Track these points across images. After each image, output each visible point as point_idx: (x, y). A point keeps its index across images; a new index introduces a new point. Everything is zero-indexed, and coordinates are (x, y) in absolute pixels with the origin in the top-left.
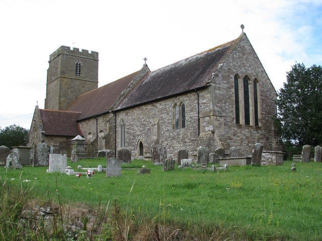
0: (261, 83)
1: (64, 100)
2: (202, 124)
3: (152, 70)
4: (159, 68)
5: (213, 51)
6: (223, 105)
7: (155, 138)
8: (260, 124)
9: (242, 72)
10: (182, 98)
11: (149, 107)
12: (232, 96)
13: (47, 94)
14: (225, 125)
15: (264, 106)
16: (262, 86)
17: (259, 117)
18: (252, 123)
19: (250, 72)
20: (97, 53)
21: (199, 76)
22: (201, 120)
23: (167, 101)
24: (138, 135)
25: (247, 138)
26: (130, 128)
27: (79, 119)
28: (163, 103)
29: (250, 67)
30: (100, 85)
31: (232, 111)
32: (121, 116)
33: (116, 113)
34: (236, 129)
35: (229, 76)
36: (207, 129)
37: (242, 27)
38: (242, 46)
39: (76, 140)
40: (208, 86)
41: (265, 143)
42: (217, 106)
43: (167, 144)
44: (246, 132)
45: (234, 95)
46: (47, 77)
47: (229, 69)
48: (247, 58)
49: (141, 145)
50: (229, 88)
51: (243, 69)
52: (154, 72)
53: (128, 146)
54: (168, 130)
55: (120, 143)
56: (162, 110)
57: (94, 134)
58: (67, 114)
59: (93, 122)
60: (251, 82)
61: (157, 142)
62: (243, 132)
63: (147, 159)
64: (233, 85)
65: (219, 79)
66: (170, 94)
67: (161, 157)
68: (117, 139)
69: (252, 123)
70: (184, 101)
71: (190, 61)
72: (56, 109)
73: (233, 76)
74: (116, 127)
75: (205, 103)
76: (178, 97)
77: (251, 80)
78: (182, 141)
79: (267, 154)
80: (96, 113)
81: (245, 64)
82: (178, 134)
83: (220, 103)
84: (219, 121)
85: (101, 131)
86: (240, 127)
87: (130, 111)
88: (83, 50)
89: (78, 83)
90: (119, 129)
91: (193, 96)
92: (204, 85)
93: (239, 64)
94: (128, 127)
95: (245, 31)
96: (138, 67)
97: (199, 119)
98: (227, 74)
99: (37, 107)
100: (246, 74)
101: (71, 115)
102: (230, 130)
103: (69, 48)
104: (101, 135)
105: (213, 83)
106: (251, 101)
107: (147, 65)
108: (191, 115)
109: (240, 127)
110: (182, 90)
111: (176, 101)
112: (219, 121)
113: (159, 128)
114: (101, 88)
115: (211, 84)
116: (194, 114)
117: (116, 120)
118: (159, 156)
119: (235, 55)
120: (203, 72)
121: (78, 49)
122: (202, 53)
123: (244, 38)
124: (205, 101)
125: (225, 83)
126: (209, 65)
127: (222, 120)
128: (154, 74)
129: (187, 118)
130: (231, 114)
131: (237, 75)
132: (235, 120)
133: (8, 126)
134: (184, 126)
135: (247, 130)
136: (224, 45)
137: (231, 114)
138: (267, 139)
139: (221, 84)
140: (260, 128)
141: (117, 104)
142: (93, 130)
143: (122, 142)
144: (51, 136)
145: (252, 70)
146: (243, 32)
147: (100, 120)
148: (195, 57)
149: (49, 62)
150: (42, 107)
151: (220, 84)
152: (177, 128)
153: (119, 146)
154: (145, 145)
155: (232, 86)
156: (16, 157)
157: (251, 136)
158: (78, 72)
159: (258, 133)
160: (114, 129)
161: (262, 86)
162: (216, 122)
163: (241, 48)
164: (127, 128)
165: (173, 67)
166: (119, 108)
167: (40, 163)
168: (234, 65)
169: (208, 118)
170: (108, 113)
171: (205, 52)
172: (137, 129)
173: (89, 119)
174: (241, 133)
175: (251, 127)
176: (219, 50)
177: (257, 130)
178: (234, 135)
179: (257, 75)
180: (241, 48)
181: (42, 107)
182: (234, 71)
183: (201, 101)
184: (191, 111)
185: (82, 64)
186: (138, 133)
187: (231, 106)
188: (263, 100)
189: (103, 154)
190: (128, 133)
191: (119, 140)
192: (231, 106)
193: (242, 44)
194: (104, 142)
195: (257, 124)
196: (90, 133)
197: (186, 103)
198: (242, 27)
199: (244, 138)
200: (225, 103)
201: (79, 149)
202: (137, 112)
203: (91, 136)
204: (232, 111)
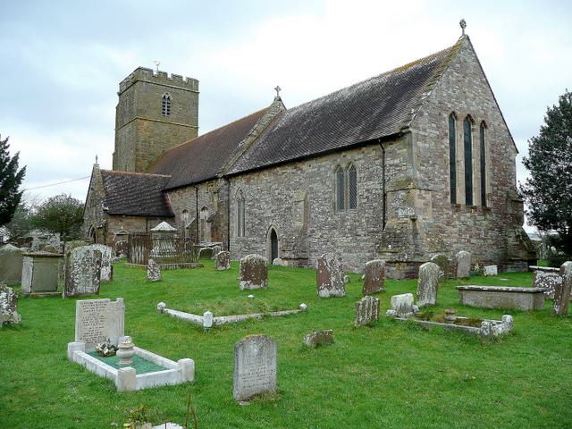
0: (491, 129)
2: (391, 204)
3: (288, 107)
7: (299, 224)
8: (489, 205)
9: (462, 108)
10: (349, 156)
11: (289, 170)
13: (116, 146)
14: (434, 205)
16: (494, 134)
17: (488, 190)
18: (476, 201)
19: (475, 109)
20: (197, 82)
21: (381, 116)
22: (389, 196)
23: (323, 159)
25: (468, 229)
27: (167, 187)
28: (314, 163)
30: (201, 133)
31: (444, 180)
32: (239, 184)
33: (228, 178)
36: (400, 213)
37: (463, 24)
39: (159, 231)
40: (404, 134)
41: (497, 237)
42: (421, 171)
44: (466, 217)
45: (448, 151)
46: (117, 118)
48: (470, 82)
49: (274, 235)
50: (440, 138)
51: (463, 102)
52: (293, 110)
53: (251, 235)
54: (323, 212)
55: (236, 229)
56: (311, 176)
57: (192, 213)
58: (148, 179)
59: (190, 192)
60: (476, 127)
61: (303, 232)
62: (462, 218)
63: (286, 263)
64: (448, 131)
65: (424, 121)
66: (329, 147)
67: (333, 279)
68: (231, 222)
69: (476, 201)
72: (130, 171)
73: (446, 116)
74: (228, 202)
75: (397, 166)
76: (343, 154)
77: (477, 126)
78: (350, 233)
79: (554, 274)
80: (196, 177)
82: (344, 221)
85: (203, 209)
86: (457, 208)
87: (255, 177)
88: (174, 76)
89: (166, 128)
90: (234, 206)
91: (372, 152)
95: (467, 31)
96: (265, 102)
97: (385, 195)
99: (96, 165)
100: (468, 112)
101: (155, 181)
103: (151, 71)
104: (204, 215)
105: (414, 128)
106: (475, 162)
107: (280, 100)
108: (368, 187)
109: (457, 208)
110: (350, 141)
111: (338, 160)
112: (424, 198)
113: (306, 206)
114: (203, 136)
115: (410, 129)
116: (375, 185)
117: (229, 190)
118: (329, 276)
120: (390, 108)
121: (165, 74)
122: (381, 76)
123: (465, 45)
124: (397, 161)
125: (433, 128)
126: (400, 95)
127: (429, 196)
128: (292, 114)
129: (359, 192)
130: (443, 186)
132: (449, 197)
133: (53, 195)
134: (353, 206)
135: (468, 215)
136: (425, 60)
138: (501, 230)
140: (489, 210)
141: (231, 163)
142: (191, 205)
143: (239, 229)
144: (121, 215)
145: (478, 104)
146: (463, 34)
147: (203, 190)
148: (369, 83)
149: (120, 95)
150: (107, 164)
151: (425, 130)
152: (341, 207)
153: (235, 235)
154: (280, 235)
155: (446, 134)
157: (475, 224)
158: (166, 111)
160: (225, 206)
161: (494, 134)
162: (419, 200)
163: (458, 61)
165: (328, 101)
166: (235, 171)
168: (449, 95)
169: (403, 193)
170: (216, 178)
171: (388, 73)
172: (266, 209)
173: (183, 187)
174: (459, 219)
175: (475, 208)
177: (484, 215)
178: (448, 224)
180: (458, 61)
181: (107, 164)
183: (389, 161)
184: (369, 179)
185: (171, 98)
187: (442, 171)
188: (494, 160)
189: (208, 254)
190: (250, 214)
191: (234, 225)
193: (462, 55)
194: (208, 228)
195: (484, 203)
196: (184, 211)
197: (359, 164)
198: (463, 24)
201: (164, 247)
202: (266, 177)
203: (186, 216)
204: (444, 180)
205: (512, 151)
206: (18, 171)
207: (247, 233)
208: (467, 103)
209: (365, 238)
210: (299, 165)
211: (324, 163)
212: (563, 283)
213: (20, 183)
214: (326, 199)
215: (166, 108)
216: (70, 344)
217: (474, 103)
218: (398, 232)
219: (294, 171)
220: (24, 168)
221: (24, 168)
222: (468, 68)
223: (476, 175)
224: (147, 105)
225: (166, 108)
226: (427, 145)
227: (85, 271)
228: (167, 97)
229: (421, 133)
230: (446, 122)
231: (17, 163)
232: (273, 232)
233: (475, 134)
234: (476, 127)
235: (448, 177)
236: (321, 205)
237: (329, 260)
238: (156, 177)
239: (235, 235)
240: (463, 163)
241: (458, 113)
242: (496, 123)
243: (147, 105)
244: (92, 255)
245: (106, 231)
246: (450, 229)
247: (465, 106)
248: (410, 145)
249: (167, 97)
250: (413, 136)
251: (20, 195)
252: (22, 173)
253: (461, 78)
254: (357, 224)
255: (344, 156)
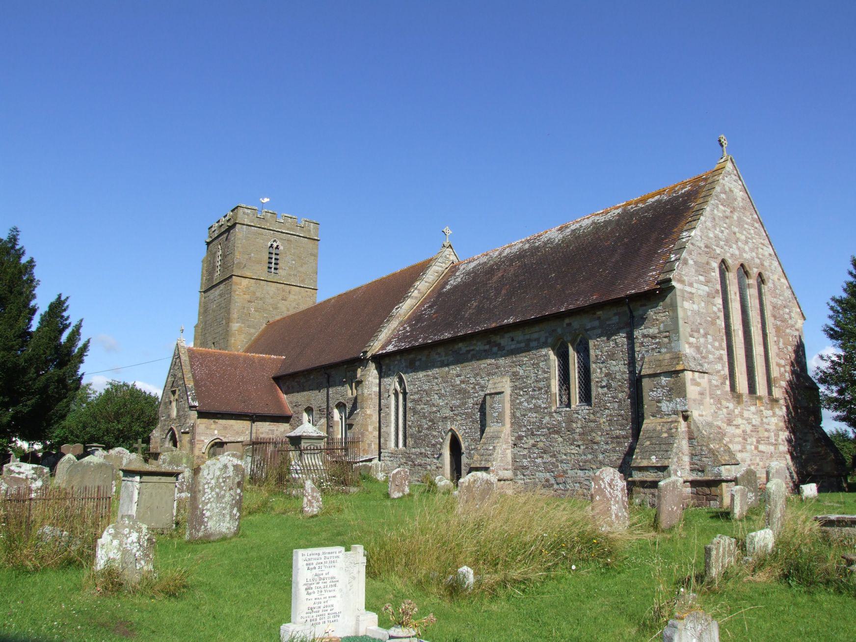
0: (770, 284)
1: (241, 327)
4: (197, 313)
5: (641, 205)
6: (702, 340)
9: (733, 254)
12: (718, 318)
15: (781, 345)
18: (761, 389)
24: (445, 418)
25: (755, 429)
26: (420, 400)
29: (746, 243)
34: (731, 406)
35: (708, 263)
36: (665, 406)
38: (727, 189)
43: (534, 445)
44: (751, 411)
45: (721, 315)
47: (706, 247)
48: (739, 218)
50: (710, 296)
62: (746, 414)
70: (588, 330)
71: (573, 231)
73: (715, 265)
75: (654, 337)
76: (567, 321)
81: (738, 234)
83: (695, 334)
84: (698, 384)
86: (738, 398)
92: (653, 286)
93: (725, 234)
94: (416, 397)
98: (704, 259)
100: (741, 261)
102: (719, 409)
112: (698, 384)
119: (715, 212)
125: (701, 283)
128: (472, 265)
130: (719, 367)
131: (723, 261)
132: (728, 382)
135: (753, 408)
137: (719, 367)
139: (695, 285)
140: (776, 401)
145: (752, 250)
151: (691, 285)
156: (134, 536)
157: (762, 423)
158: (273, 265)
159: (774, 414)
164: (414, 400)
165: (527, 246)
167: (210, 524)
168: (716, 236)
176: (658, 201)
177: (772, 409)
178: (729, 422)
179: (762, 265)
182: (718, 251)
185: (281, 248)
186: (447, 413)
187: (717, 344)
192: (717, 344)
195: (752, 388)
199: (749, 428)
200: (705, 335)
204: (720, 358)
205: (797, 316)
206: (80, 344)
207: (410, 442)
208: (739, 248)
209: (609, 447)
210: (497, 339)
211: (535, 336)
212: (207, 539)
213: (82, 362)
214: (540, 389)
215: (273, 261)
216: (284, 627)
217: (747, 248)
218: (665, 435)
219: (487, 347)
220: (89, 341)
221: (89, 341)
222: (735, 199)
223: (758, 350)
224: (246, 257)
225: (273, 261)
226: (695, 307)
227: (220, 498)
228: (275, 245)
229: (688, 289)
230: (716, 274)
231: (79, 334)
232: (175, 445)
233: (752, 293)
234: (752, 281)
235: (724, 353)
236: (533, 397)
237: (607, 479)
238: (263, 359)
239: (392, 444)
240: (740, 333)
241: (730, 261)
242: (775, 277)
243: (246, 257)
244: (231, 471)
245: (193, 438)
246: (731, 430)
247: (737, 252)
248: (673, 307)
249: (275, 245)
250: (678, 293)
251: (81, 378)
252: (85, 347)
253: (728, 214)
254: (592, 425)
255: (569, 325)
